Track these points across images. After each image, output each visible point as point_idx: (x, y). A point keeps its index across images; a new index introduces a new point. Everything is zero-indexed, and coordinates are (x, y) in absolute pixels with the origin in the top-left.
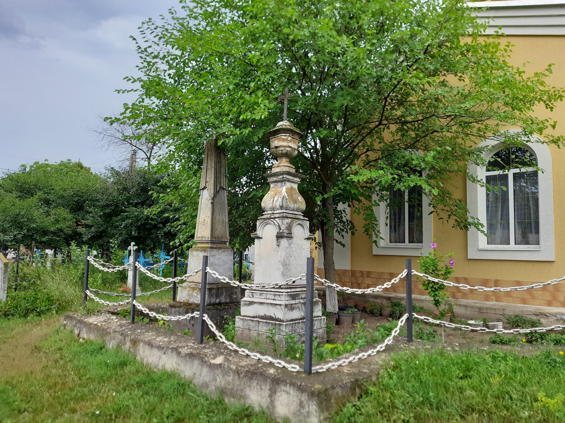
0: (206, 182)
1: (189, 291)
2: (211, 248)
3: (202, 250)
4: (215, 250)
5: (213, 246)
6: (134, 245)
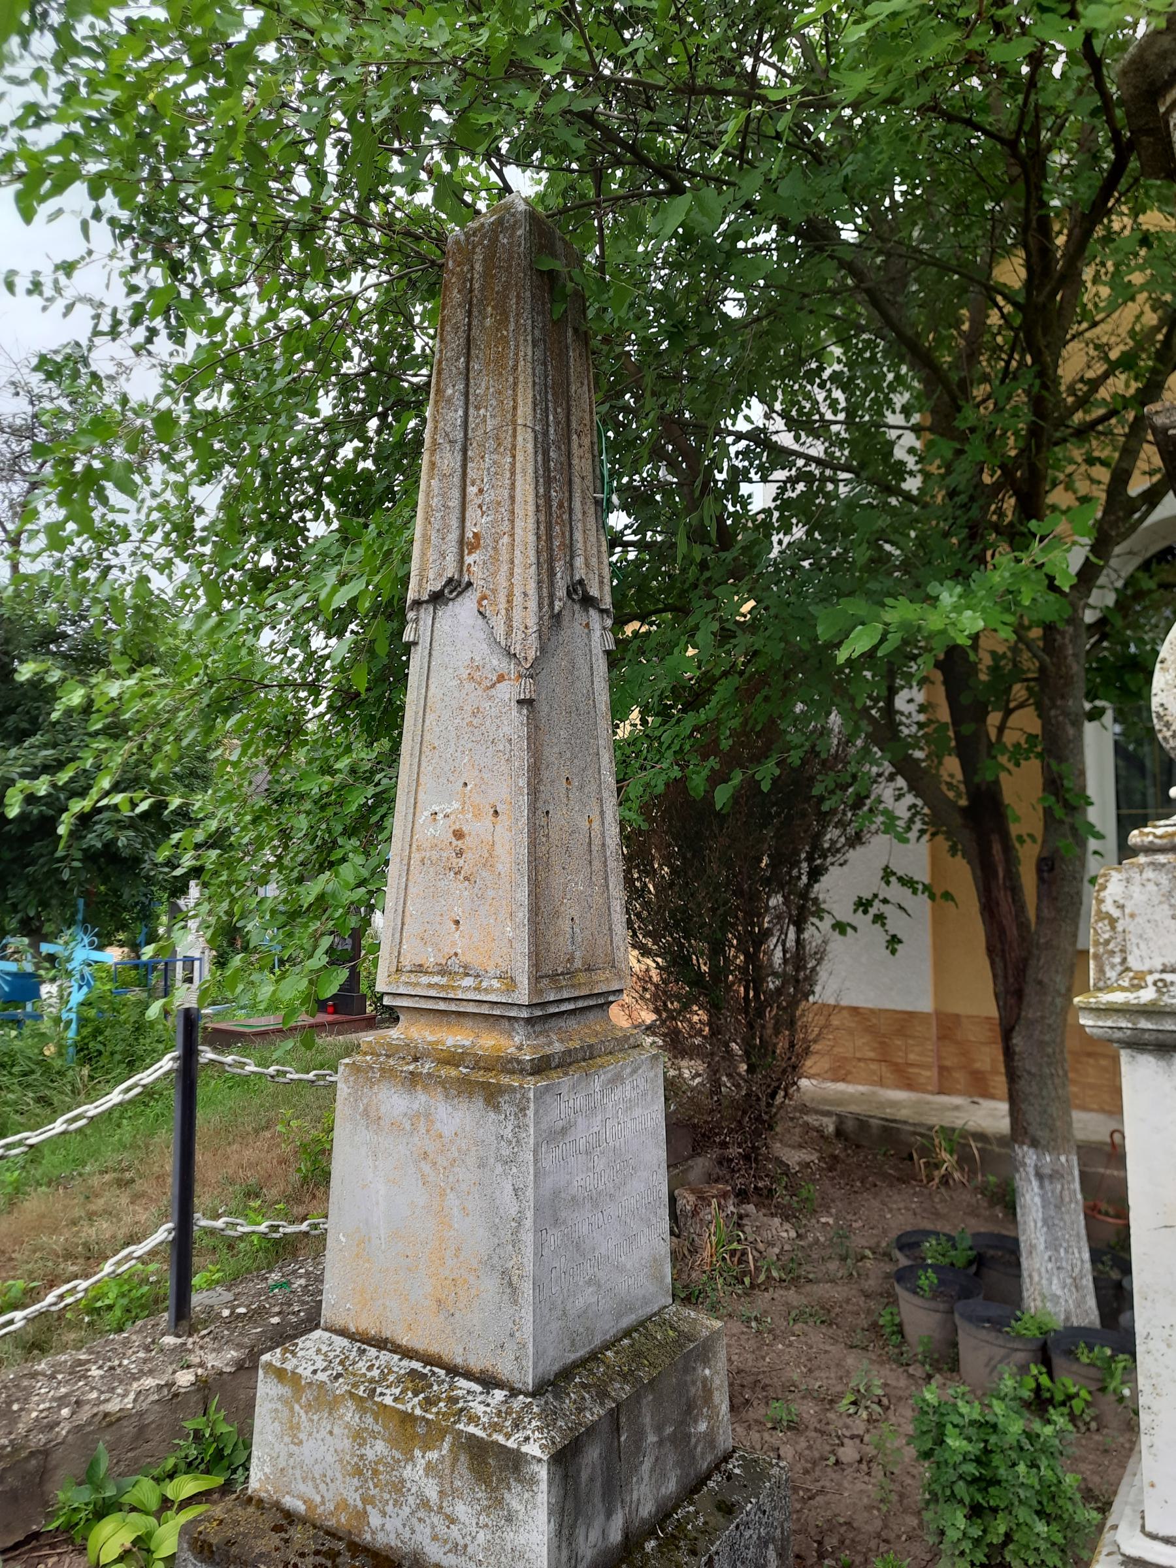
0: (465, 545)
1: (360, 1437)
2: (541, 1067)
3: (465, 1088)
4: (565, 1082)
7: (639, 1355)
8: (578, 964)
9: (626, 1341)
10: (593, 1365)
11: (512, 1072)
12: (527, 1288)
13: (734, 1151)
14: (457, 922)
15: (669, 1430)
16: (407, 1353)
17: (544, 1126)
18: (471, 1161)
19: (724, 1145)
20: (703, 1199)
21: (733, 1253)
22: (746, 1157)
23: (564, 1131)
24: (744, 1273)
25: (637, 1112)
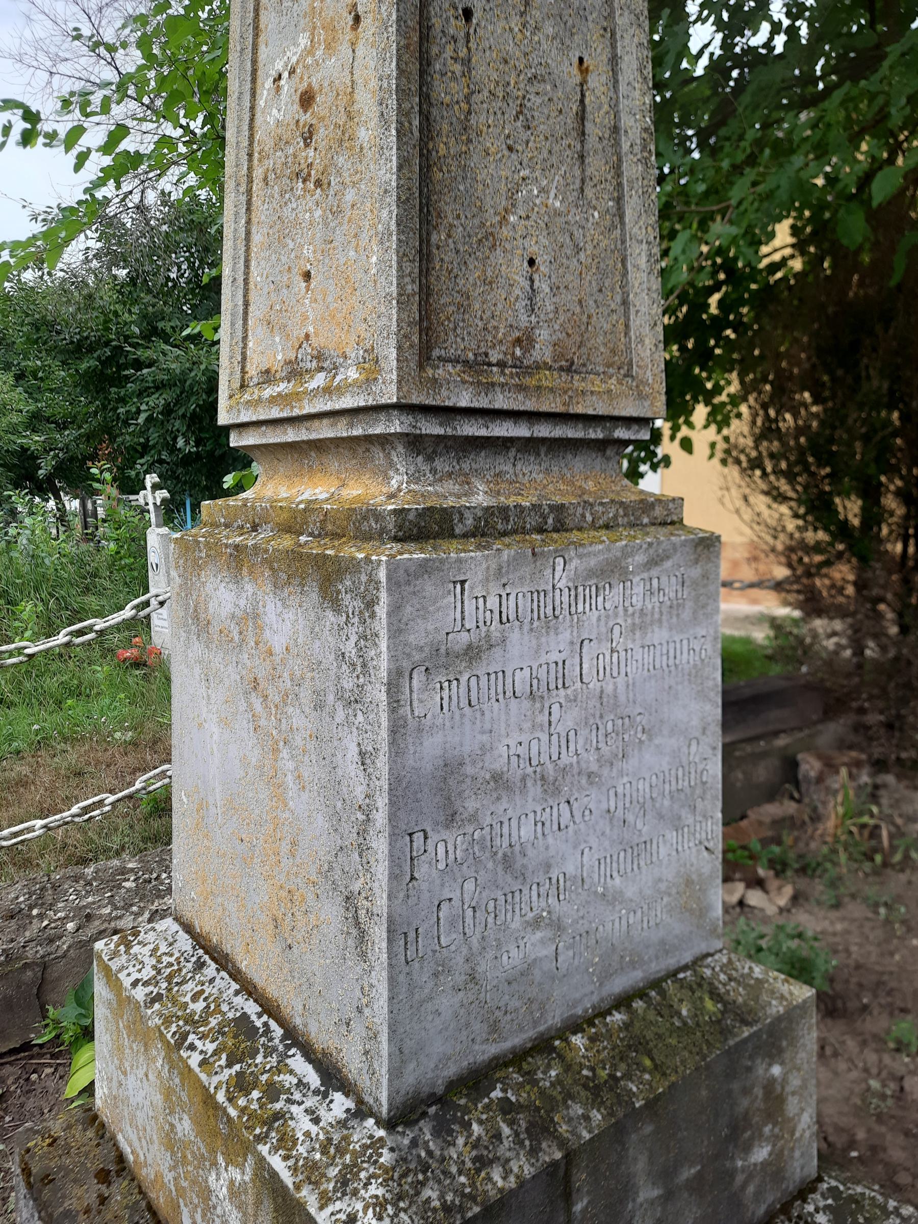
4: (476, 562)
5: (445, 494)
6: (155, 487)
7: (639, 1045)
8: (542, 352)
9: (618, 1017)
10: (540, 1061)
11: (367, 537)
12: (378, 934)
13: (874, 718)
14: (307, 276)
15: (688, 1172)
16: (248, 989)
17: (417, 636)
18: (306, 695)
19: (862, 711)
20: (831, 766)
21: (863, 826)
22: (890, 726)
23: (472, 653)
24: (875, 850)
25: (658, 635)
